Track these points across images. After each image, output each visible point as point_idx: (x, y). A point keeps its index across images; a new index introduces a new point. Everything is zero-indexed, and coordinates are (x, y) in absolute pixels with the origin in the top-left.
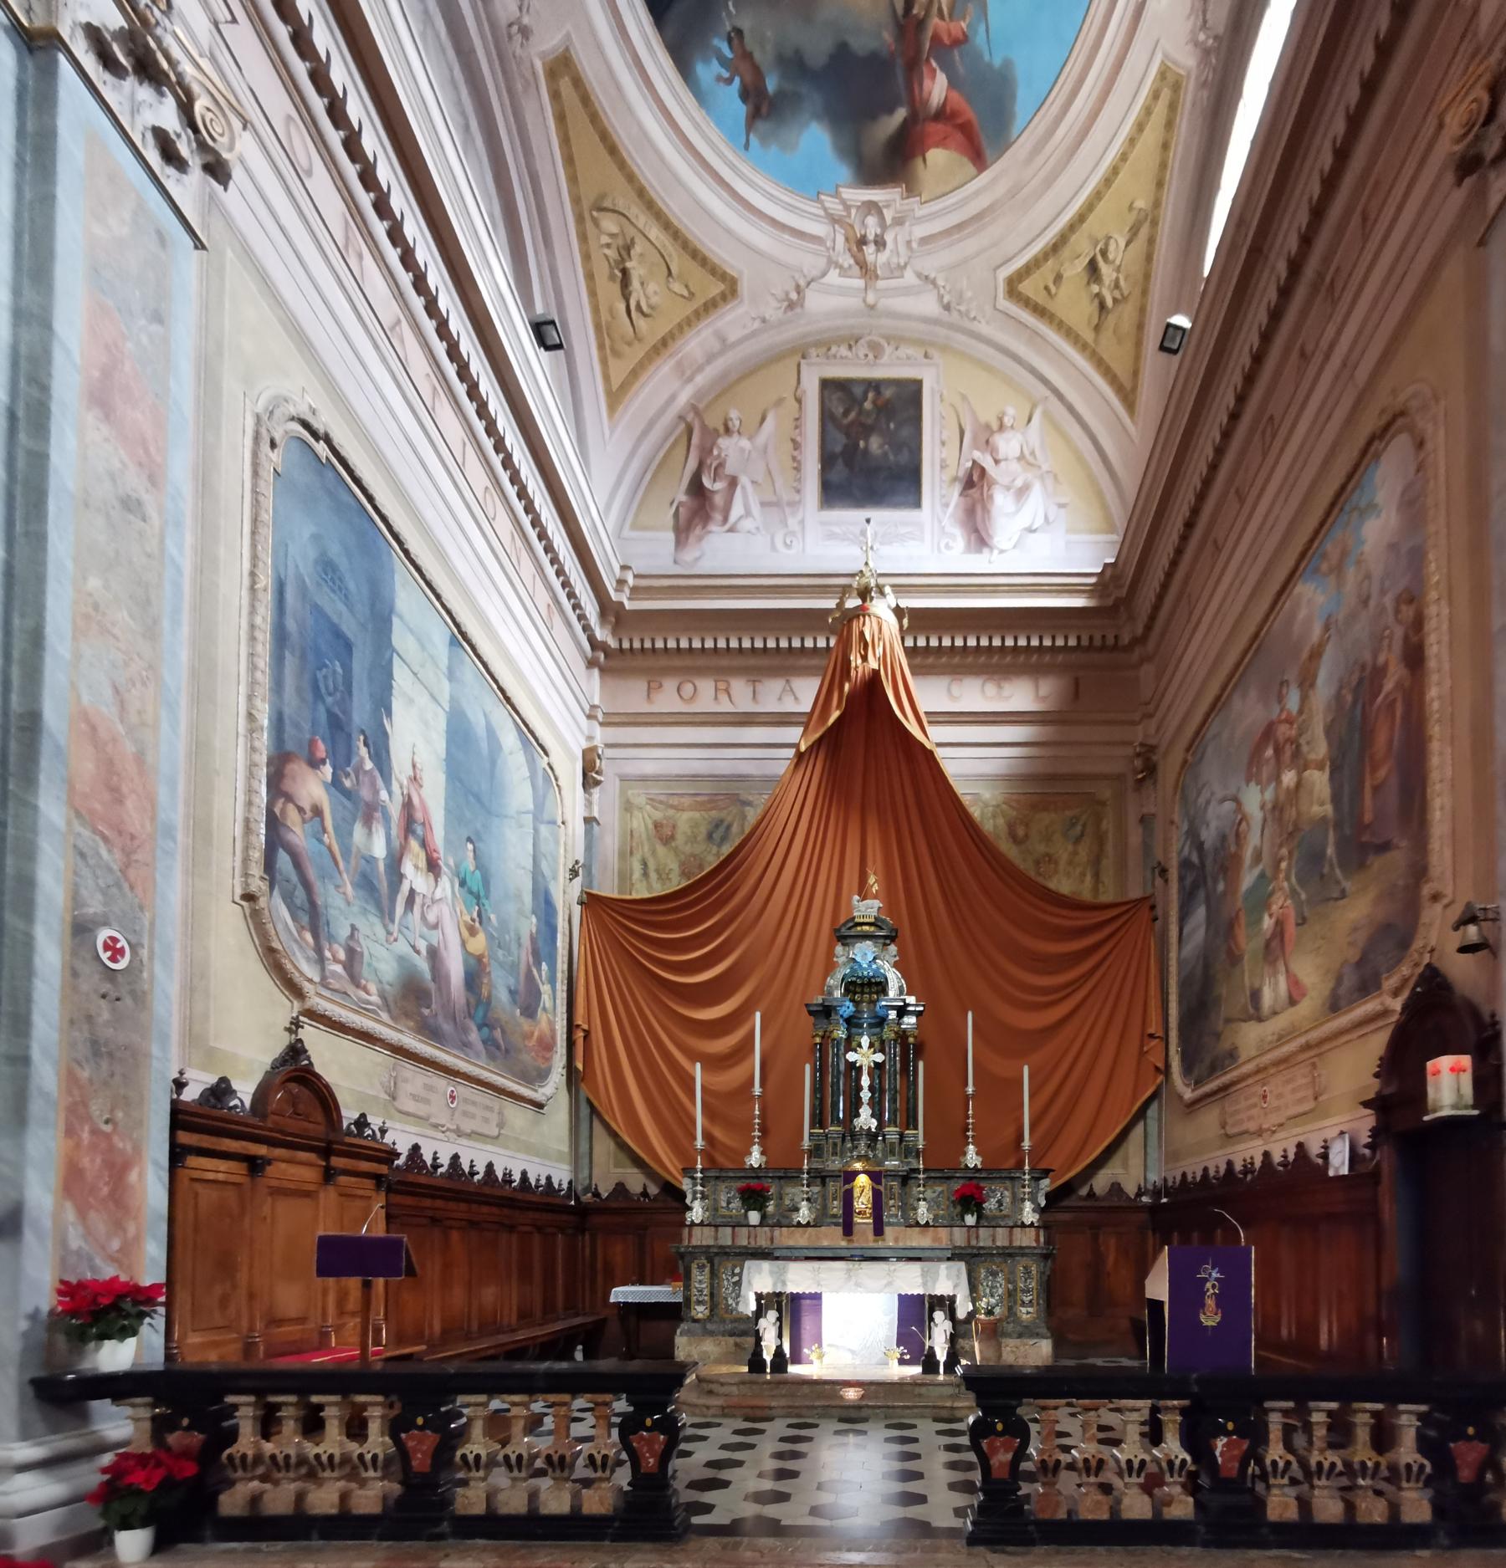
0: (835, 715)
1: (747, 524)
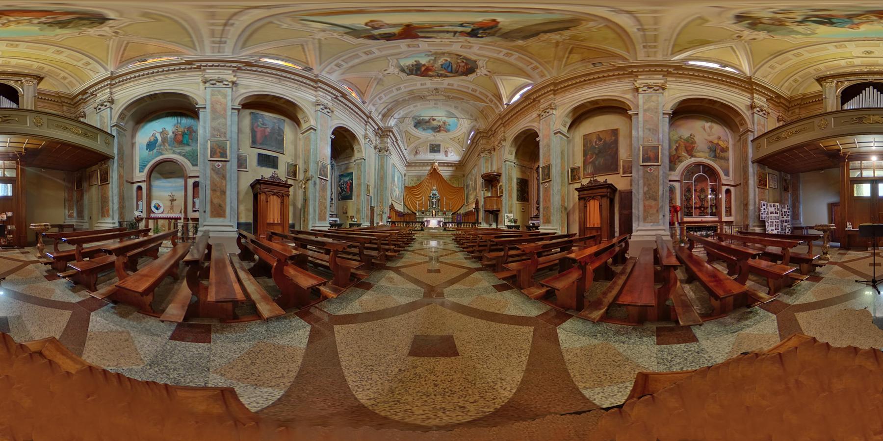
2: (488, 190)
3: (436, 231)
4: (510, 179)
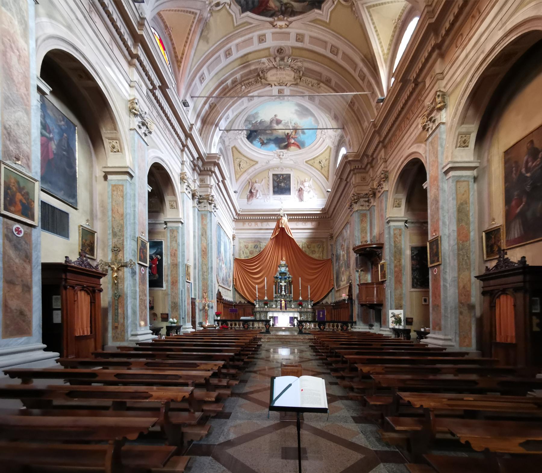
0: (277, 233)
1: (260, 198)
2: (365, 270)
3: (287, 333)
4: (398, 253)
